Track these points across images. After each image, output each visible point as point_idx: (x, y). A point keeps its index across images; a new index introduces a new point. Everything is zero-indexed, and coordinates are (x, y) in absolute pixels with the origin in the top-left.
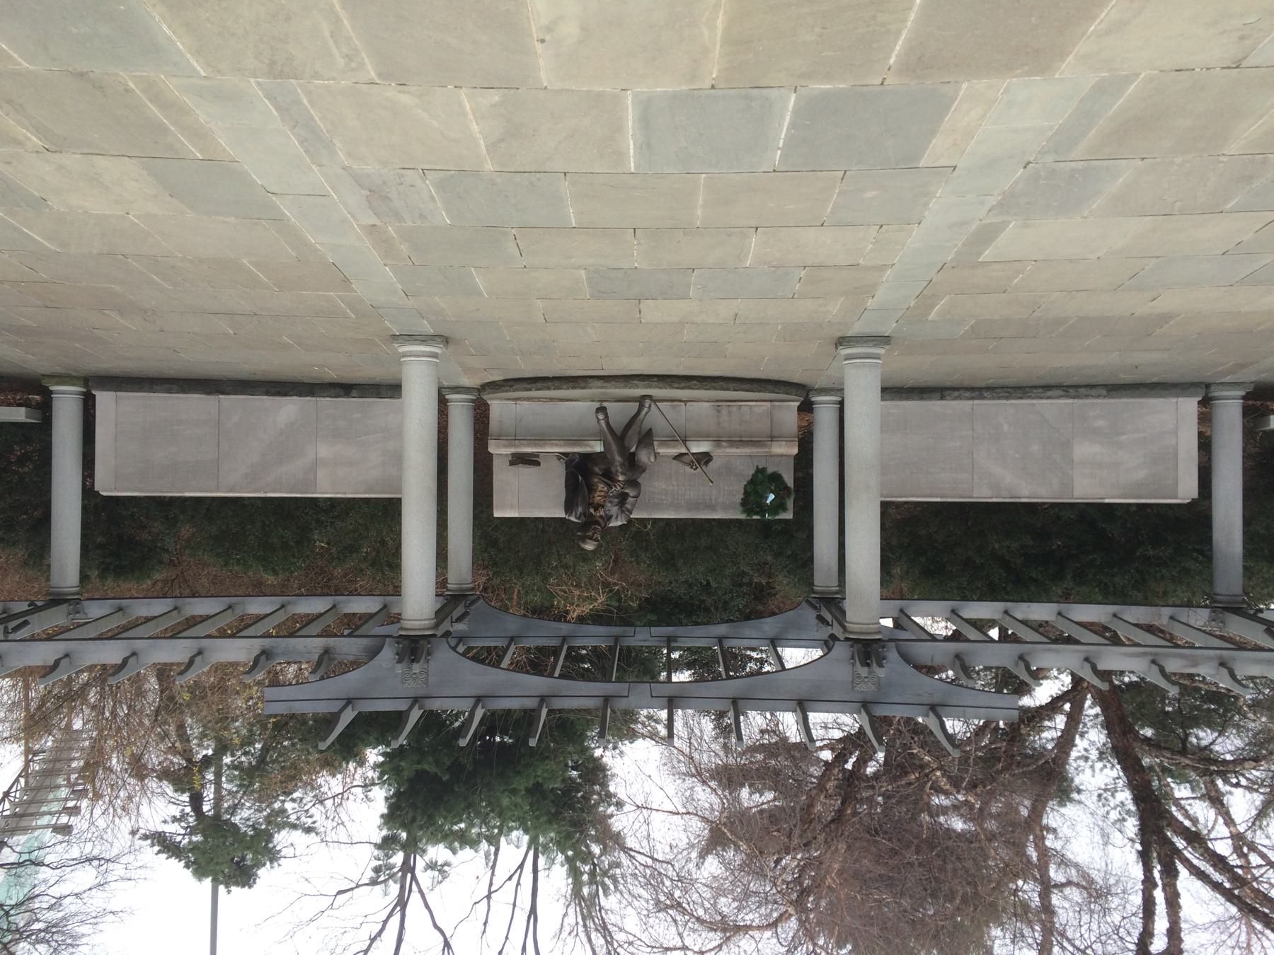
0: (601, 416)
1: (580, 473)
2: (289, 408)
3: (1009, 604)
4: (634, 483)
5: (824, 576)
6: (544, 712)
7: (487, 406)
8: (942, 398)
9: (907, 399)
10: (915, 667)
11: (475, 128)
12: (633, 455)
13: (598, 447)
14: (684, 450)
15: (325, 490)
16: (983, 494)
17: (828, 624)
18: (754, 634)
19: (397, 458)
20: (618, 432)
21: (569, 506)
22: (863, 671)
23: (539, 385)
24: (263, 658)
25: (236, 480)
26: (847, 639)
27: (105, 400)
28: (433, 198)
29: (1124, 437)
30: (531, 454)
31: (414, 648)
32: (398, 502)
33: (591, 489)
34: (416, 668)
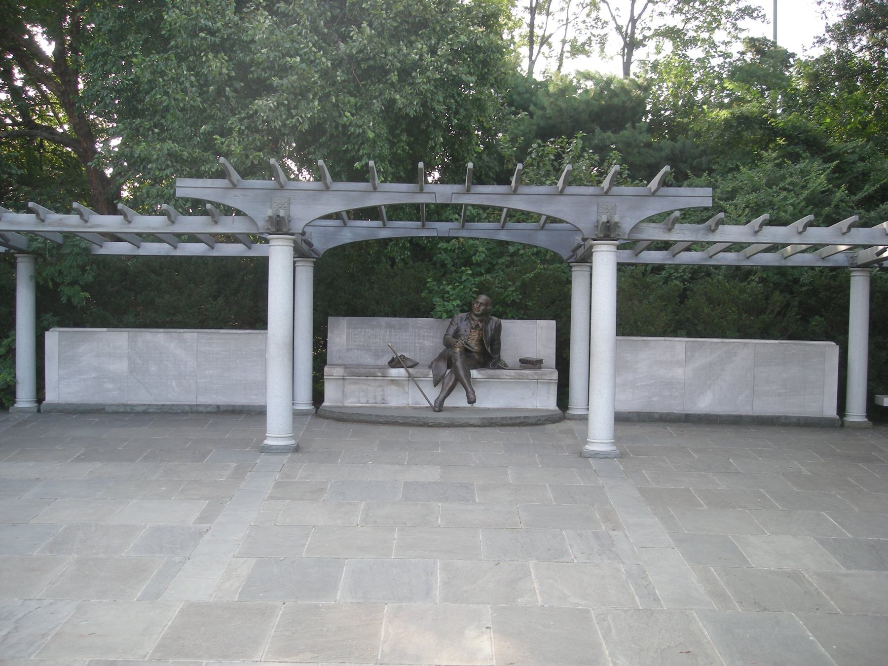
0: (471, 396)
1: (488, 355)
2: (704, 404)
3: (173, 254)
4: (448, 345)
5: (306, 273)
6: (513, 184)
7: (558, 405)
8: (218, 407)
9: (243, 406)
10: (245, 215)
11: (536, 585)
12: (448, 367)
13: (474, 373)
14: (410, 370)
15: (679, 345)
16: (190, 336)
17: (305, 241)
18: (359, 230)
19: (619, 366)
20: (459, 385)
21: (498, 329)
22: (282, 213)
23: (518, 421)
24: (713, 228)
25: (743, 353)
26: (292, 234)
27: (831, 411)
28: (571, 547)
29: (94, 375)
30: (525, 368)
31: (608, 231)
32: (618, 333)
33: (481, 341)
34: (604, 219)
